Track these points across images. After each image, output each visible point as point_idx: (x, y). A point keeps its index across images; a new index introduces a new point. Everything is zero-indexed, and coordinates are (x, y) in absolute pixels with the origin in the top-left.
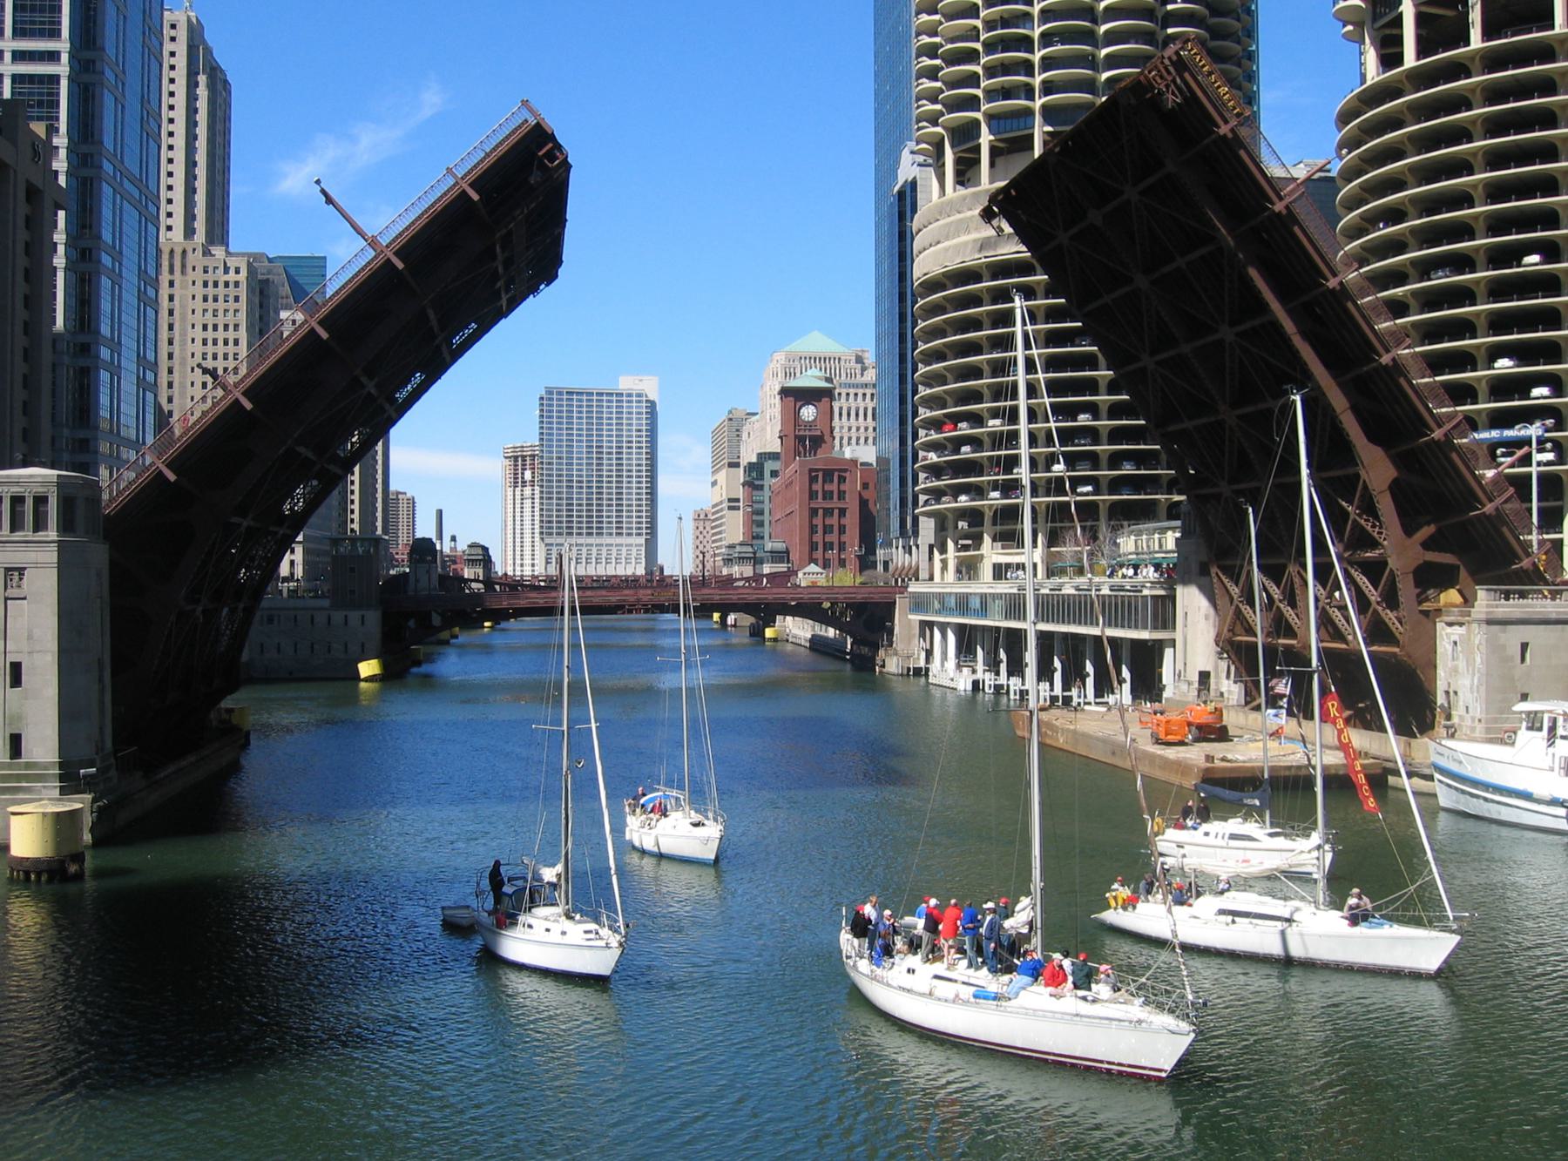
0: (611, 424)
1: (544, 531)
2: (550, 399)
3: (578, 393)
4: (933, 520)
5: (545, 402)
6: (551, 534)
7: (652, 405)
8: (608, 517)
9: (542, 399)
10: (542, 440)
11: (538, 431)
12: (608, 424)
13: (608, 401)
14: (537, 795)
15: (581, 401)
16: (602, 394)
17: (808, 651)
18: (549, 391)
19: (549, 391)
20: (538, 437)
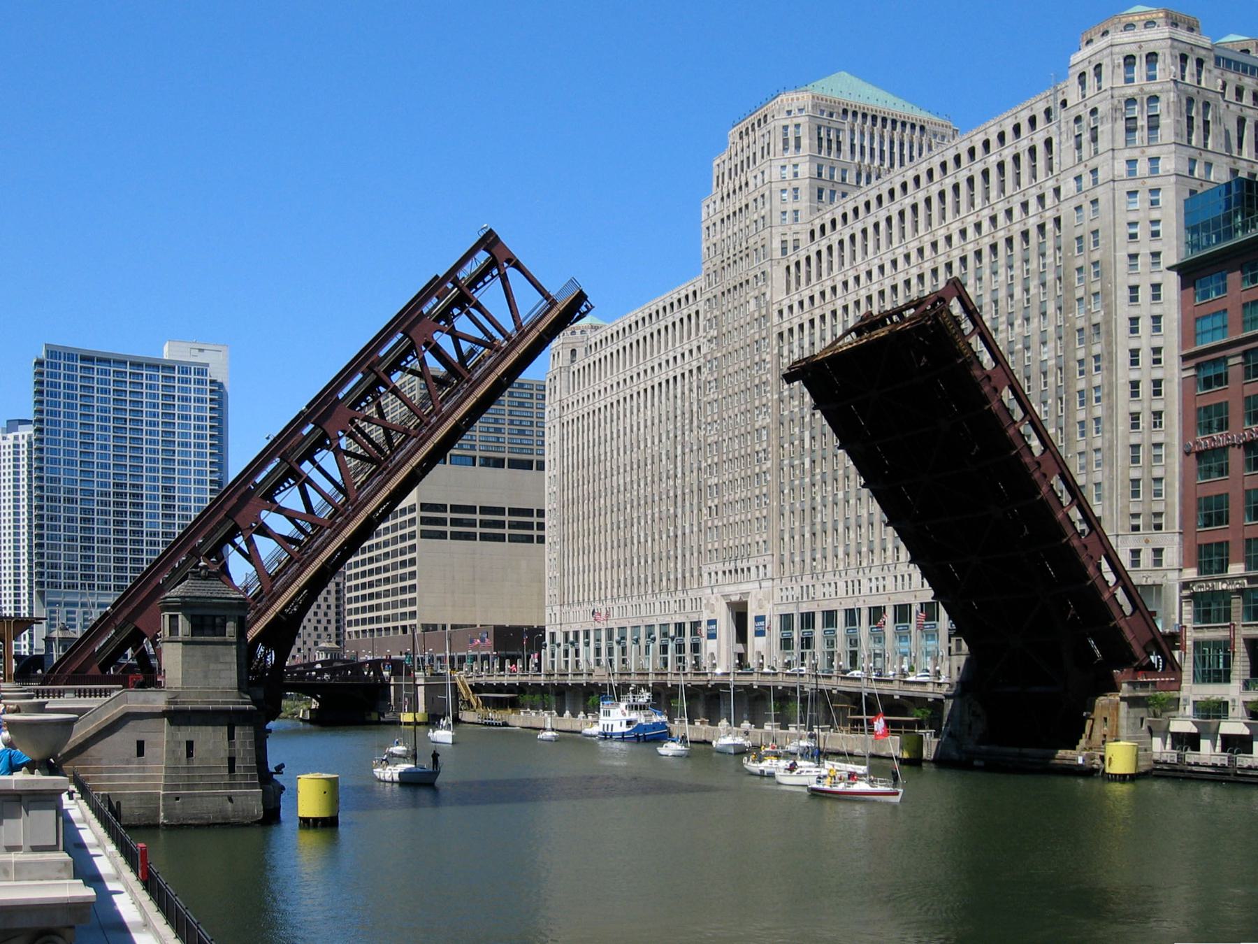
0: (154, 461)
1: (45, 579)
2: (54, 366)
3: (100, 360)
4: (1175, 273)
5: (45, 369)
6: (57, 586)
7: (218, 389)
8: (150, 424)
9: (39, 363)
10: (40, 412)
11: (31, 379)
12: (150, 424)
13: (150, 377)
14: (1203, 717)
15: (106, 373)
16: (139, 365)
17: (396, 786)
18: (53, 352)
19: (53, 352)
20: (32, 409)
